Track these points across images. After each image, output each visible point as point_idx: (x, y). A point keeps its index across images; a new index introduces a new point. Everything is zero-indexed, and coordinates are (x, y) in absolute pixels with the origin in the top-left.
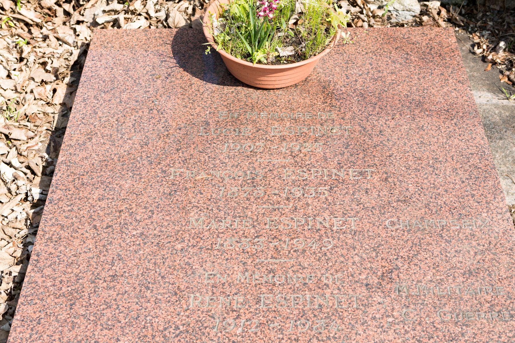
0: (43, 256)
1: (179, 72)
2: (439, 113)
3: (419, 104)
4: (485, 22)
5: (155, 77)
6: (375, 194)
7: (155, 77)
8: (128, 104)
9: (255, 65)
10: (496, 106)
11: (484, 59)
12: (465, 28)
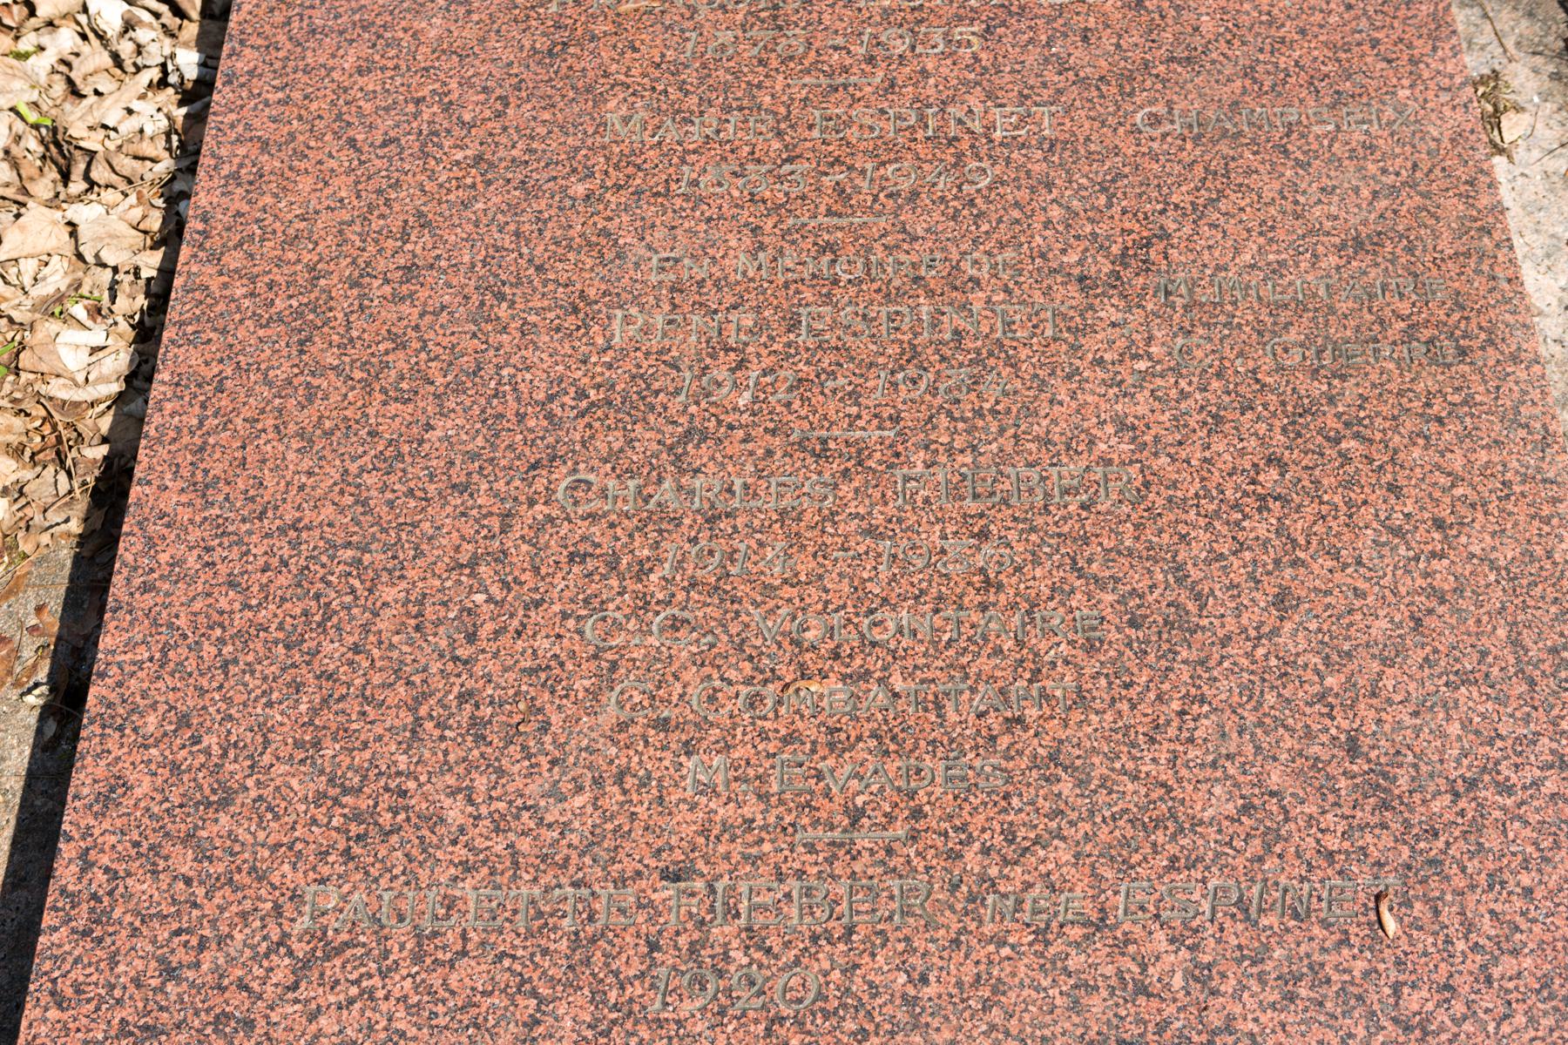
0: (221, 219)
6: (1108, 43)
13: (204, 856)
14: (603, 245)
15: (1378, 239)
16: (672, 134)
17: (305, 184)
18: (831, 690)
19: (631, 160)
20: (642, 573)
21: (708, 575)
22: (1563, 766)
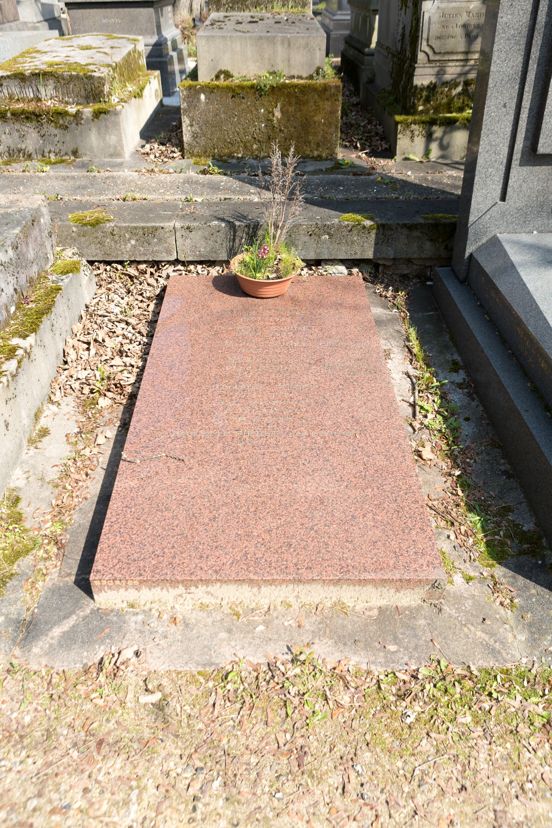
0: (155, 354)
1: (217, 292)
2: (350, 308)
3: (340, 304)
4: (383, 280)
5: (204, 294)
6: (315, 335)
7: (204, 294)
8: (52, 668)
9: (257, 280)
10: (385, 314)
11: (381, 295)
12: (372, 282)
13: (155, 428)
14: (224, 358)
15: (362, 359)
16: (237, 345)
17: (170, 350)
18: (265, 410)
19: (230, 348)
20: (231, 396)
21: (244, 396)
22: (551, 603)
